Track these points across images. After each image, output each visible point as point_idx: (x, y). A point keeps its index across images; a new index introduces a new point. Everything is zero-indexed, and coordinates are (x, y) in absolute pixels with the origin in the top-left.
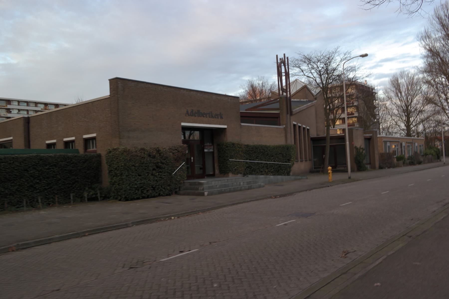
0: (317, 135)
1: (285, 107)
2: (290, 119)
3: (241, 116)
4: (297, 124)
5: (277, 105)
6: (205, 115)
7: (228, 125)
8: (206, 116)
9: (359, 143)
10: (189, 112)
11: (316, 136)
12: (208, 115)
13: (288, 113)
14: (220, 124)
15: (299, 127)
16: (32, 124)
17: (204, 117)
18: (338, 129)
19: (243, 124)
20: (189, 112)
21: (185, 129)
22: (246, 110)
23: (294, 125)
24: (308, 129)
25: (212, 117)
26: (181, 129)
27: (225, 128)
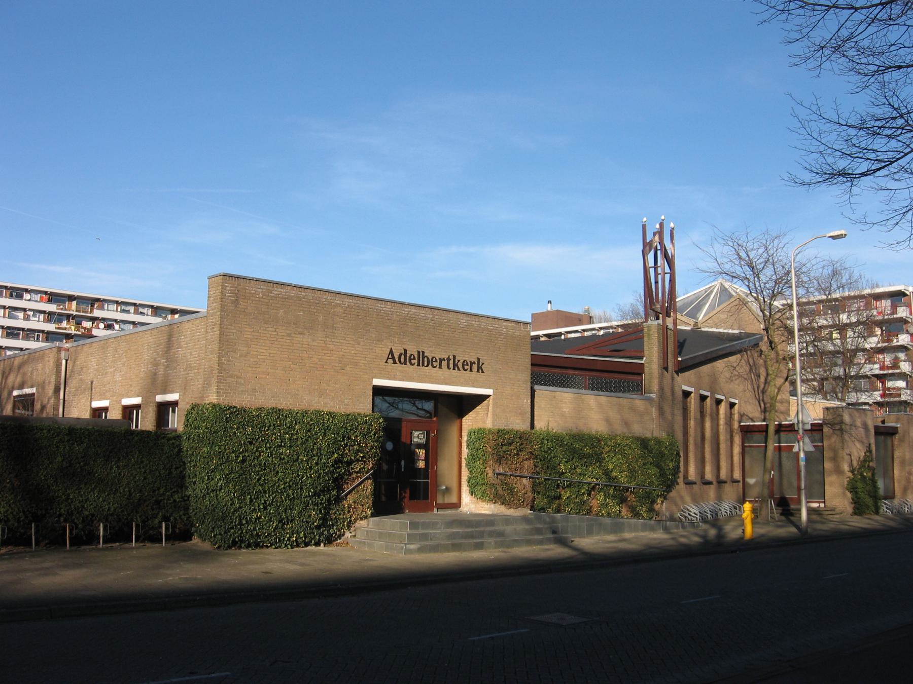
7: (495, 390)
12: (444, 363)
16: (675, 232)
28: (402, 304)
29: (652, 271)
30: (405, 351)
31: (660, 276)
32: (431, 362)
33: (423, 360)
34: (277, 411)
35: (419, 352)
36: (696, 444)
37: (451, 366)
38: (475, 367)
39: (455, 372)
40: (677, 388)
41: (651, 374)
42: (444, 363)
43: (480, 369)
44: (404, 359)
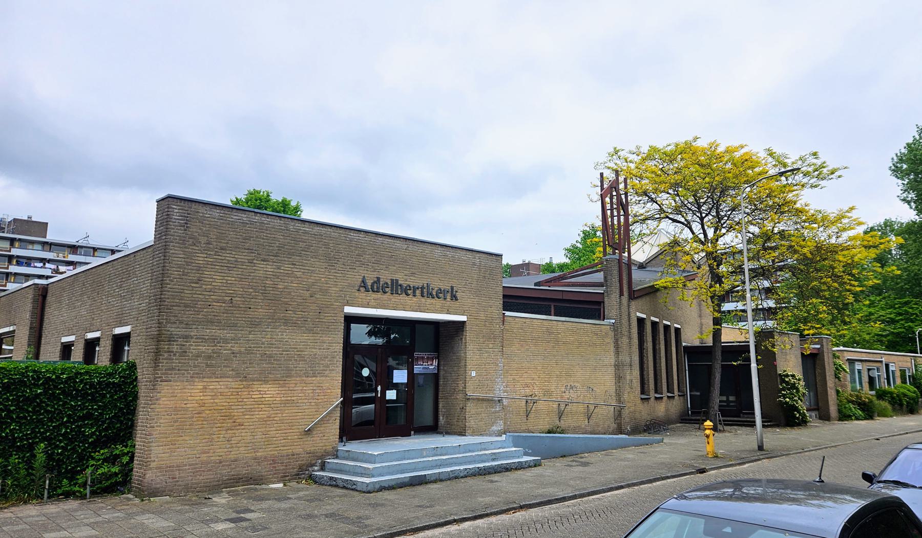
0: (702, 341)
1: (616, 279)
2: (629, 306)
3: (504, 296)
4: (661, 320)
5: (599, 277)
6: (441, 295)
7: (469, 316)
8: (414, 292)
9: (790, 365)
10: (369, 283)
11: (697, 343)
12: (418, 292)
13: (621, 294)
14: (448, 313)
15: (654, 324)
16: (49, 299)
17: (408, 295)
18: (730, 335)
19: (507, 313)
20: (369, 283)
21: (350, 320)
22: (536, 284)
23: (641, 321)
24: (677, 330)
25: (430, 295)
26: (342, 320)
27: (464, 322)
28: (377, 234)
29: (609, 212)
30: (378, 279)
31: (616, 218)
32: (406, 290)
33: (396, 288)
34: (136, 397)
35: (392, 280)
36: (661, 370)
37: (425, 294)
38: (449, 297)
39: (430, 301)
40: (632, 315)
41: (892, 490)
42: (418, 292)
43: (454, 298)
44: (377, 287)
